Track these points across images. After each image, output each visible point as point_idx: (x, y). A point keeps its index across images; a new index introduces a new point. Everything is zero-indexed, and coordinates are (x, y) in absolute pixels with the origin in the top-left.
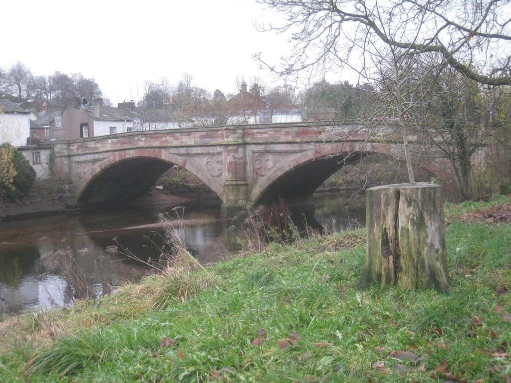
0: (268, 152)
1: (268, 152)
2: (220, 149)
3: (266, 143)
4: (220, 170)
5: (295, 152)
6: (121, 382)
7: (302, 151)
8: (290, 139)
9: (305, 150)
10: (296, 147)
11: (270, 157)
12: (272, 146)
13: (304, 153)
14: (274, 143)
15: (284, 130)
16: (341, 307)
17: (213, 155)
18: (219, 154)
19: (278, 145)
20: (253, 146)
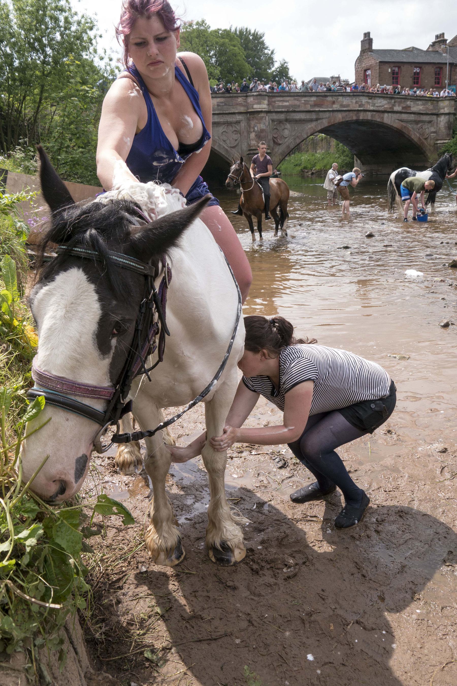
0: (287, 120)
1: (287, 120)
2: (238, 117)
3: (288, 112)
4: (236, 140)
5: (311, 121)
6: (3, 310)
7: (317, 120)
8: (309, 108)
9: (320, 119)
10: (314, 116)
11: (288, 126)
12: (293, 114)
13: (319, 122)
14: (294, 112)
15: (304, 99)
16: (4, 347)
17: (229, 124)
18: (238, 122)
19: (297, 114)
20: (274, 114)
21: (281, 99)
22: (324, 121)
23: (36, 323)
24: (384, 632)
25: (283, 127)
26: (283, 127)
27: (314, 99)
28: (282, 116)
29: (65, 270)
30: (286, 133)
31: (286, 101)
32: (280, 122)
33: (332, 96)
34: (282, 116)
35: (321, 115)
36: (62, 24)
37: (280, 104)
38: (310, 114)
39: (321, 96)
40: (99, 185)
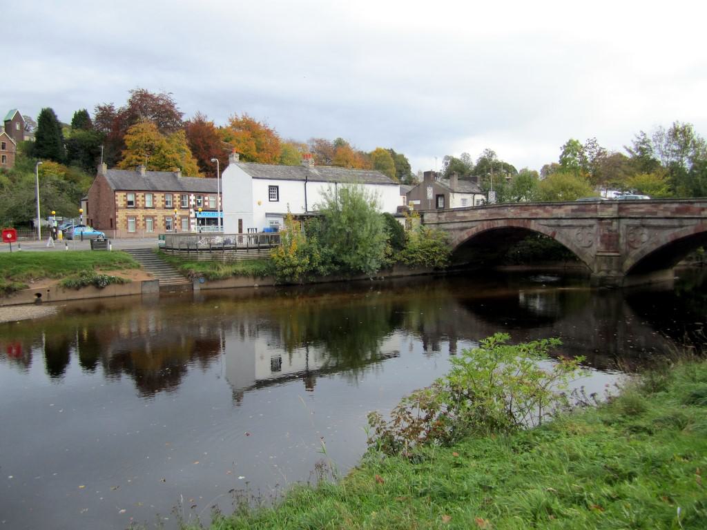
0: (644, 226)
5: (674, 227)
8: (669, 214)
10: (676, 223)
11: (646, 231)
13: (683, 229)
17: (583, 227)
18: (591, 226)
21: (635, 206)
22: (689, 228)
23: (118, 283)
24: (251, 417)
25: (641, 232)
26: (641, 232)
27: (676, 205)
28: (637, 222)
29: (56, 116)
30: (645, 238)
31: (642, 208)
32: (637, 227)
33: (700, 202)
34: (637, 222)
35: (685, 222)
36: (60, 233)
37: (635, 210)
38: (671, 220)
39: (684, 202)
40: (560, 340)
